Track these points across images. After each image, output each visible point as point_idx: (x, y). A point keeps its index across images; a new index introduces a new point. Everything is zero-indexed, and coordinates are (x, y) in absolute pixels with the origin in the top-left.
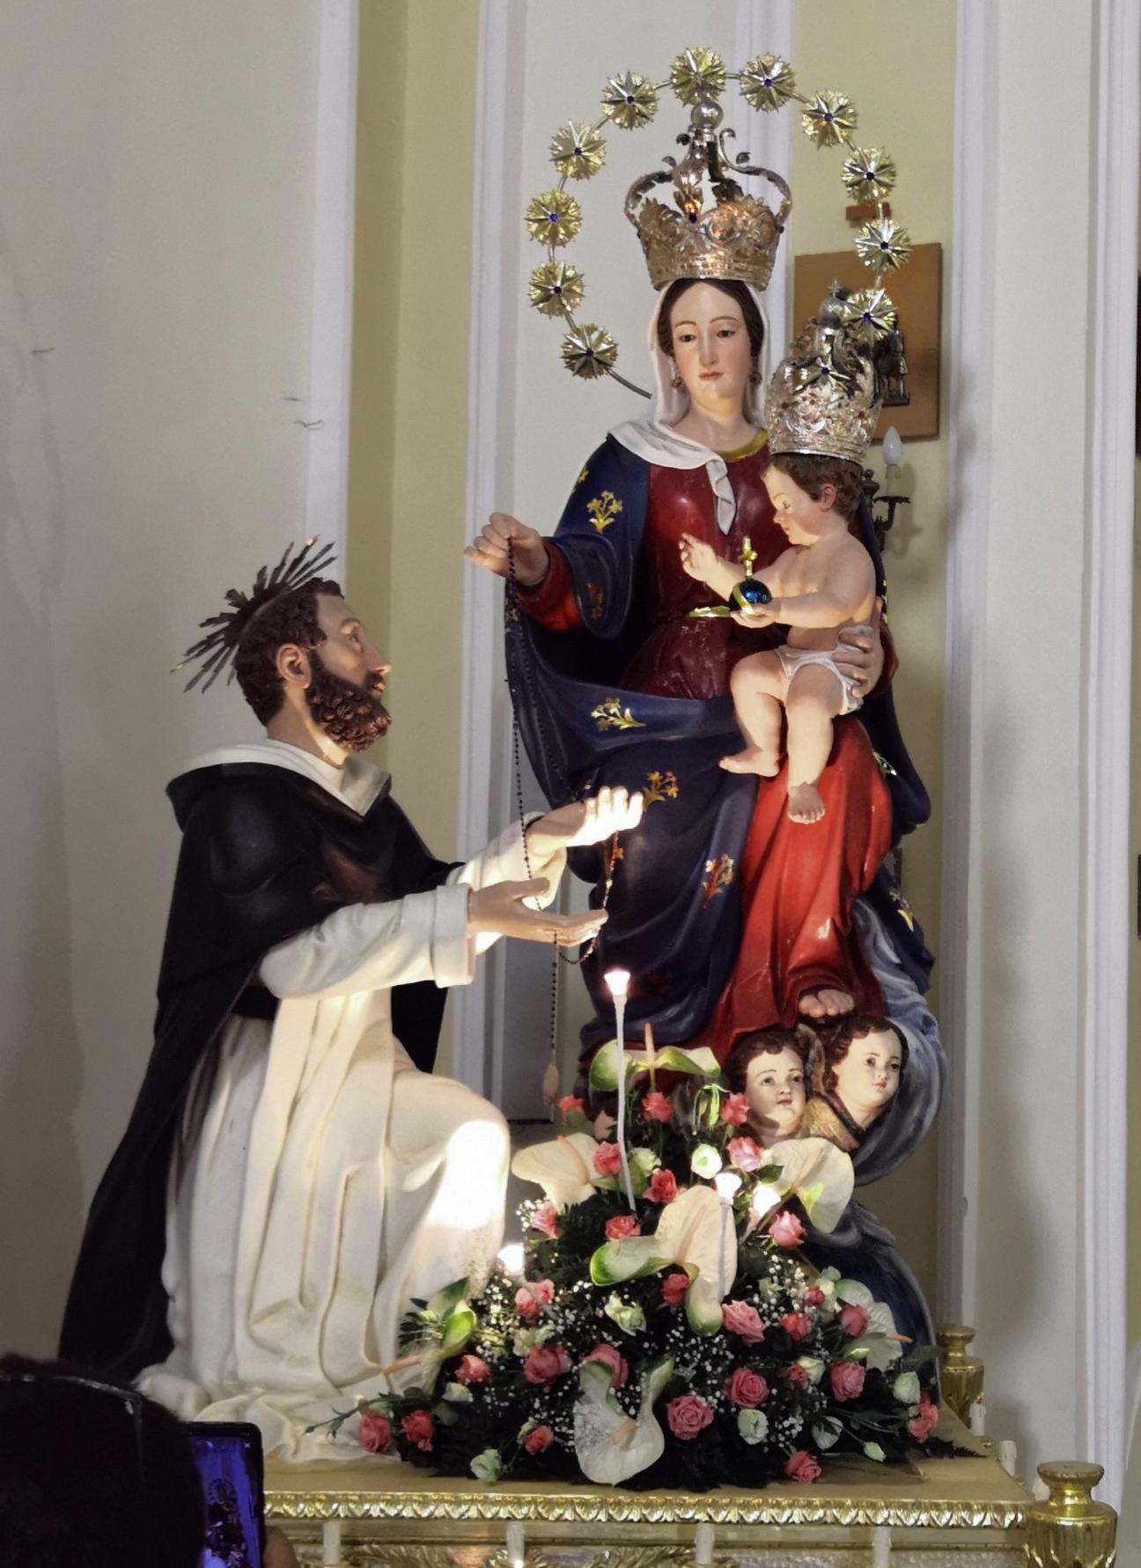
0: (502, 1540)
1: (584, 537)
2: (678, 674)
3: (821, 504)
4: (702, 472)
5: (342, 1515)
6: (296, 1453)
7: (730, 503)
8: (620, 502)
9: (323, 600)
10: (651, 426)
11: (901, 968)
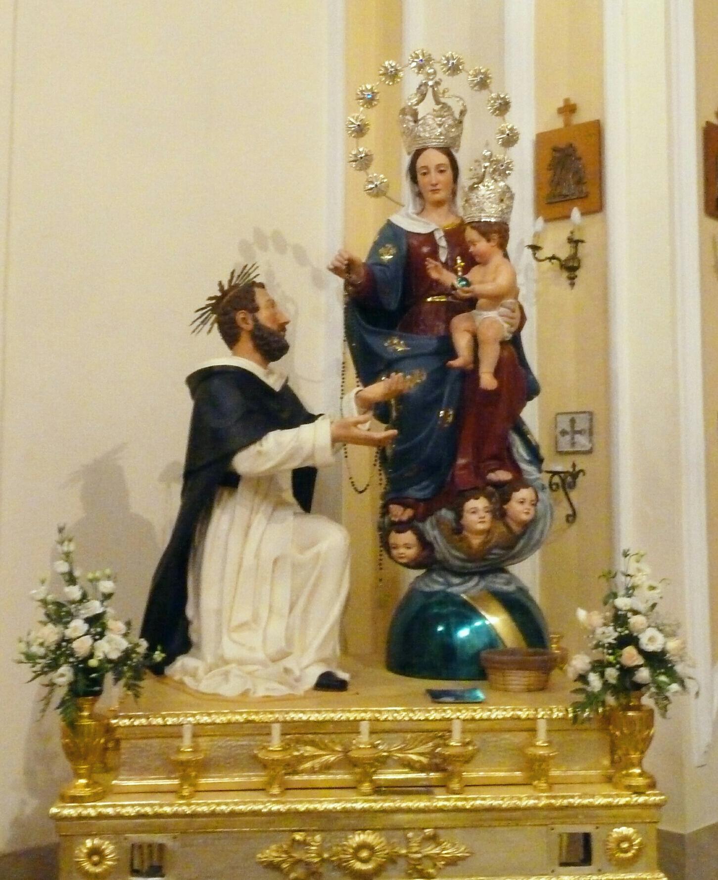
3: (492, 244)
4: (431, 235)
9: (257, 290)
11: (530, 462)
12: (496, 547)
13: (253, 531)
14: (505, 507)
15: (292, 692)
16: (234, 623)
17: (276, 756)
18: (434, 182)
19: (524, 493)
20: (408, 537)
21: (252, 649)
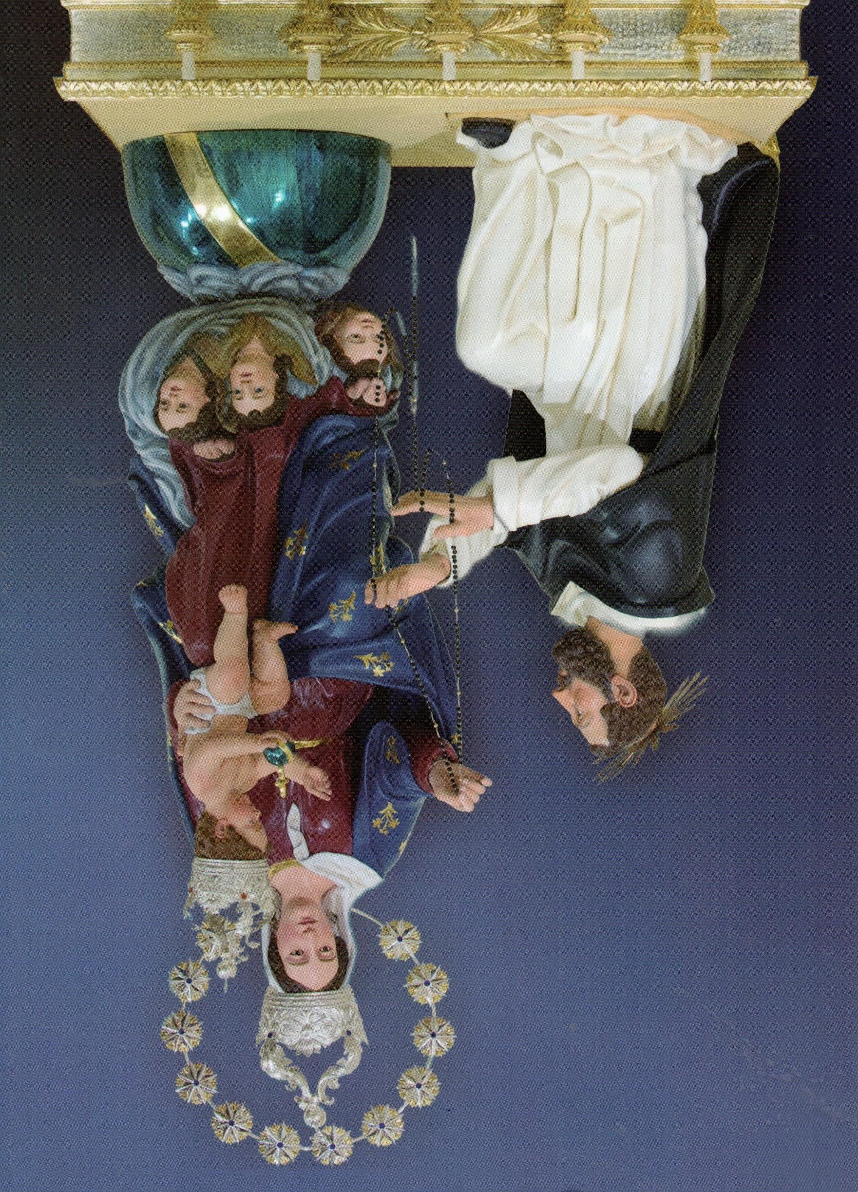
0: (458, 65)
1: (398, 798)
2: (328, 696)
3: (225, 823)
5: (571, 83)
6: (607, 120)
7: (291, 828)
8: (374, 826)
10: (351, 885)
11: (153, 475)
12: (222, 336)
13: (610, 364)
14: (208, 400)
15: (552, 120)
16: (636, 221)
17: (579, 35)
18: (310, 935)
19: (174, 420)
20: (357, 354)
21: (608, 182)
